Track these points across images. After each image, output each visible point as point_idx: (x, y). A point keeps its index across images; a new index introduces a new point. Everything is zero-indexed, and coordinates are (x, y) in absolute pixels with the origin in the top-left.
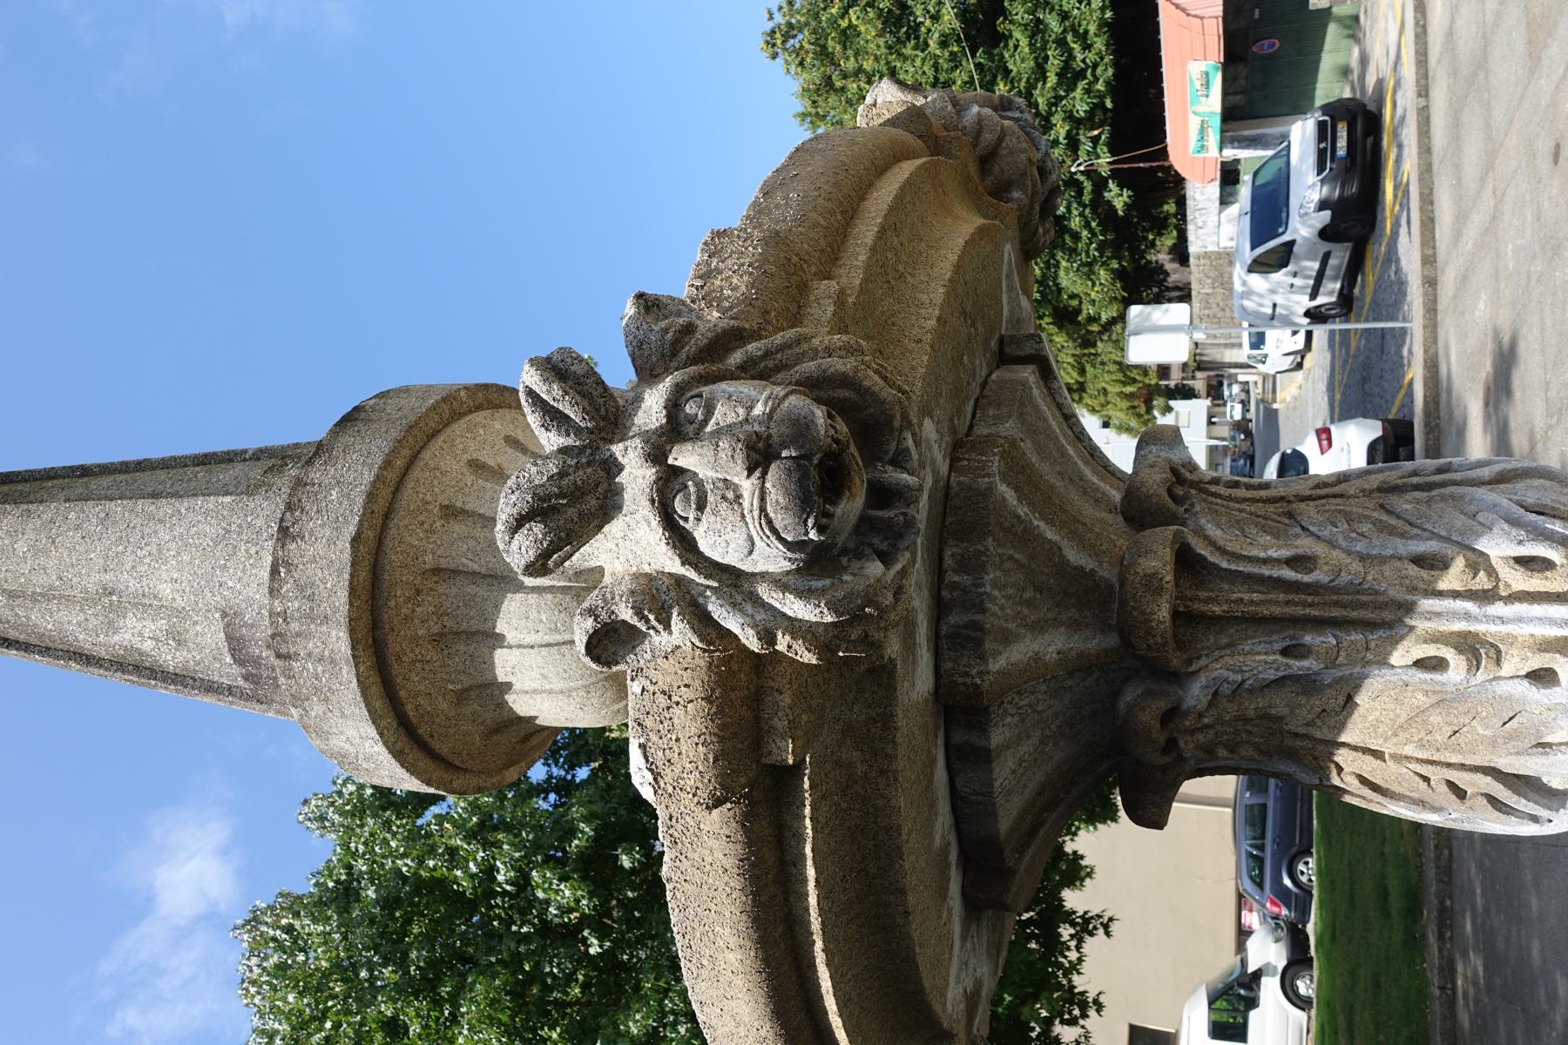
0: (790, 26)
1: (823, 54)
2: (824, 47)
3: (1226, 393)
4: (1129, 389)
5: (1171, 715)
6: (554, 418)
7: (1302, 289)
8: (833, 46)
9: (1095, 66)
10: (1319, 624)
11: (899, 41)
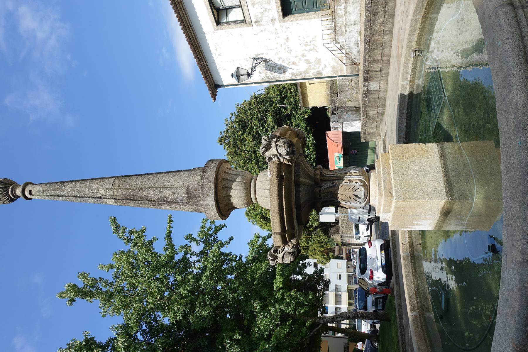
0: (227, 137)
1: (236, 145)
2: (236, 143)
3: (352, 257)
4: (322, 249)
5: (320, 191)
6: (265, 140)
7: (365, 214)
8: (238, 142)
9: (311, 154)
10: (335, 180)
11: (257, 143)
